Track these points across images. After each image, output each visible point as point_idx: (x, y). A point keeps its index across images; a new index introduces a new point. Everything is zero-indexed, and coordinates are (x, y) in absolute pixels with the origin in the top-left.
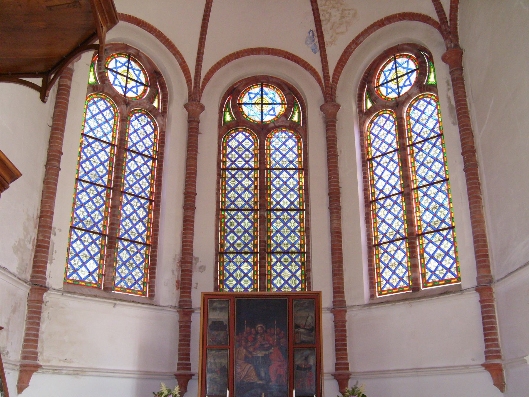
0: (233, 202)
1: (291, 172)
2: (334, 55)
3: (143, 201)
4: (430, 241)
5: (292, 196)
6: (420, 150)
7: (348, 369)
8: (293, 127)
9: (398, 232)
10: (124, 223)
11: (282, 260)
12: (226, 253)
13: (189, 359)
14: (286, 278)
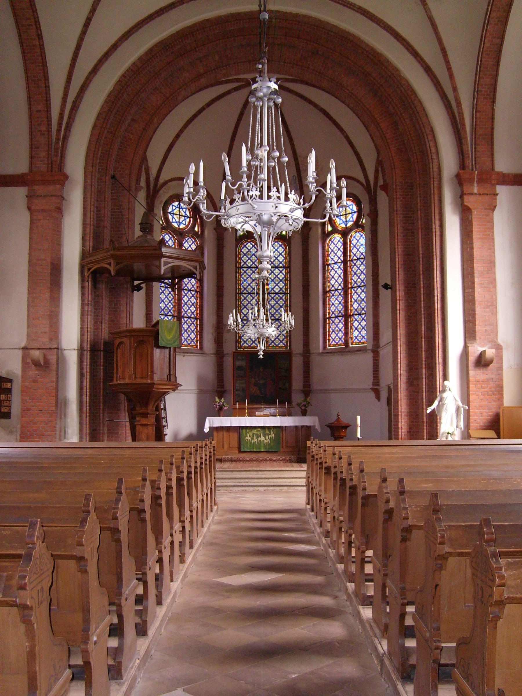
0: (245, 289)
1: (281, 269)
3: (193, 293)
4: (356, 320)
5: (281, 285)
7: (310, 387)
9: (340, 312)
13: (223, 382)
14: (277, 287)
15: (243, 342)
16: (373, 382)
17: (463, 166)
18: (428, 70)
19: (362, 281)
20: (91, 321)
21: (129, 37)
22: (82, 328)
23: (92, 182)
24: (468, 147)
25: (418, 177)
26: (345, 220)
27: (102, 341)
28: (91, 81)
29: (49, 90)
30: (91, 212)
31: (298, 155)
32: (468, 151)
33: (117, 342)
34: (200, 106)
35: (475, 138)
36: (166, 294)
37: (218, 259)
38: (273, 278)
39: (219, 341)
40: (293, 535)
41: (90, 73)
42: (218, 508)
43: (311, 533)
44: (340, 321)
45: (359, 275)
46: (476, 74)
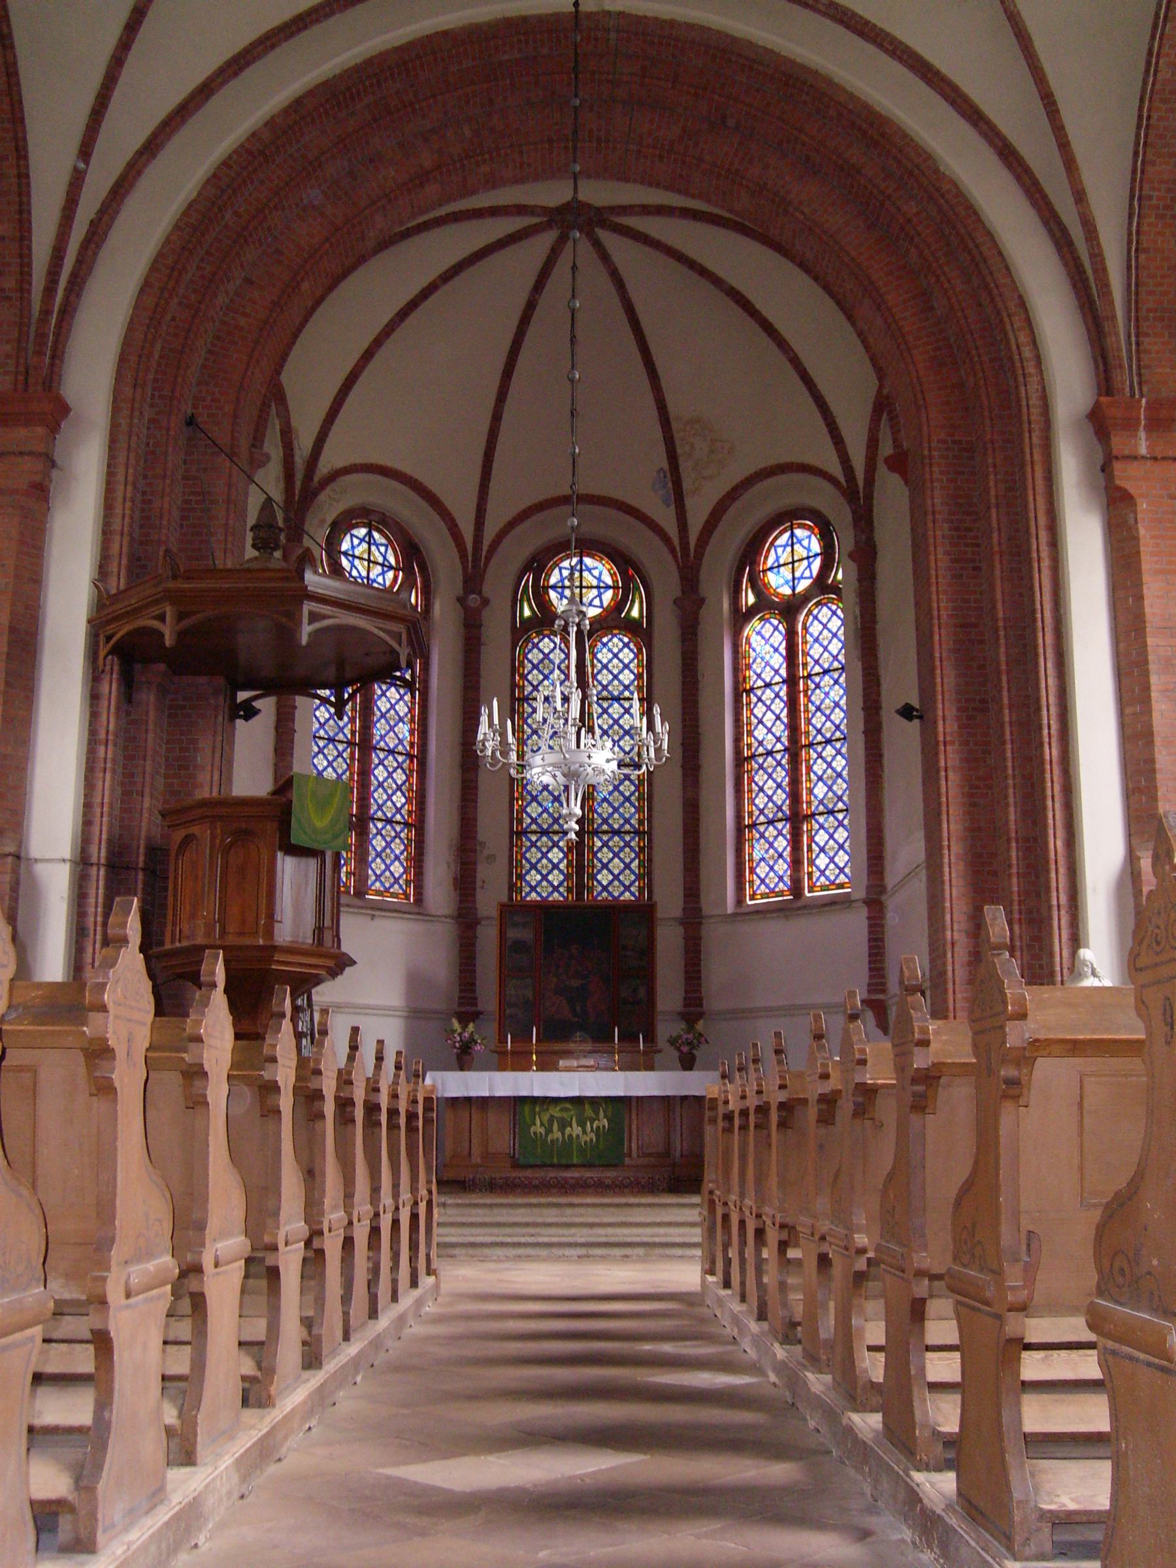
2: (698, 511)
3: (400, 759)
4: (822, 827)
6: (818, 686)
7: (701, 1005)
8: (631, 628)
9: (780, 808)
10: (376, 795)
11: (611, 844)
12: (524, 832)
13: (474, 991)
14: (616, 872)
15: (528, 889)
16: (869, 985)
17: (1105, 383)
18: (1008, 155)
19: (838, 727)
20: (112, 790)
21: (241, 69)
22: (88, 806)
23: (131, 425)
24: (1118, 341)
25: (987, 422)
26: (796, 547)
27: (142, 842)
28: (140, 173)
29: (28, 185)
30: (124, 500)
31: (672, 415)
32: (1119, 349)
33: (179, 835)
34: (425, 282)
35: (1137, 319)
36: (330, 758)
37: (465, 676)
38: (605, 727)
39: (465, 883)
40: (668, 1348)
41: (140, 153)
42: (437, 1286)
43: (727, 1343)
44: (780, 833)
45: (828, 712)
46: (1136, 154)
